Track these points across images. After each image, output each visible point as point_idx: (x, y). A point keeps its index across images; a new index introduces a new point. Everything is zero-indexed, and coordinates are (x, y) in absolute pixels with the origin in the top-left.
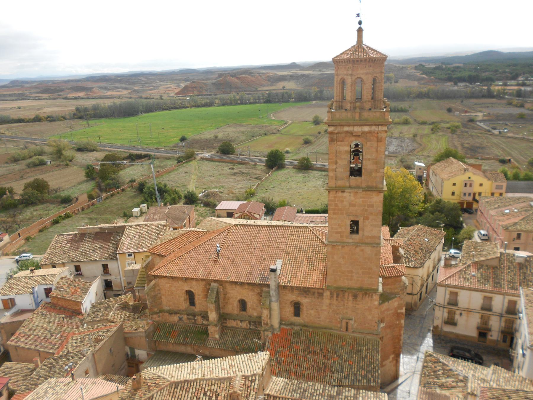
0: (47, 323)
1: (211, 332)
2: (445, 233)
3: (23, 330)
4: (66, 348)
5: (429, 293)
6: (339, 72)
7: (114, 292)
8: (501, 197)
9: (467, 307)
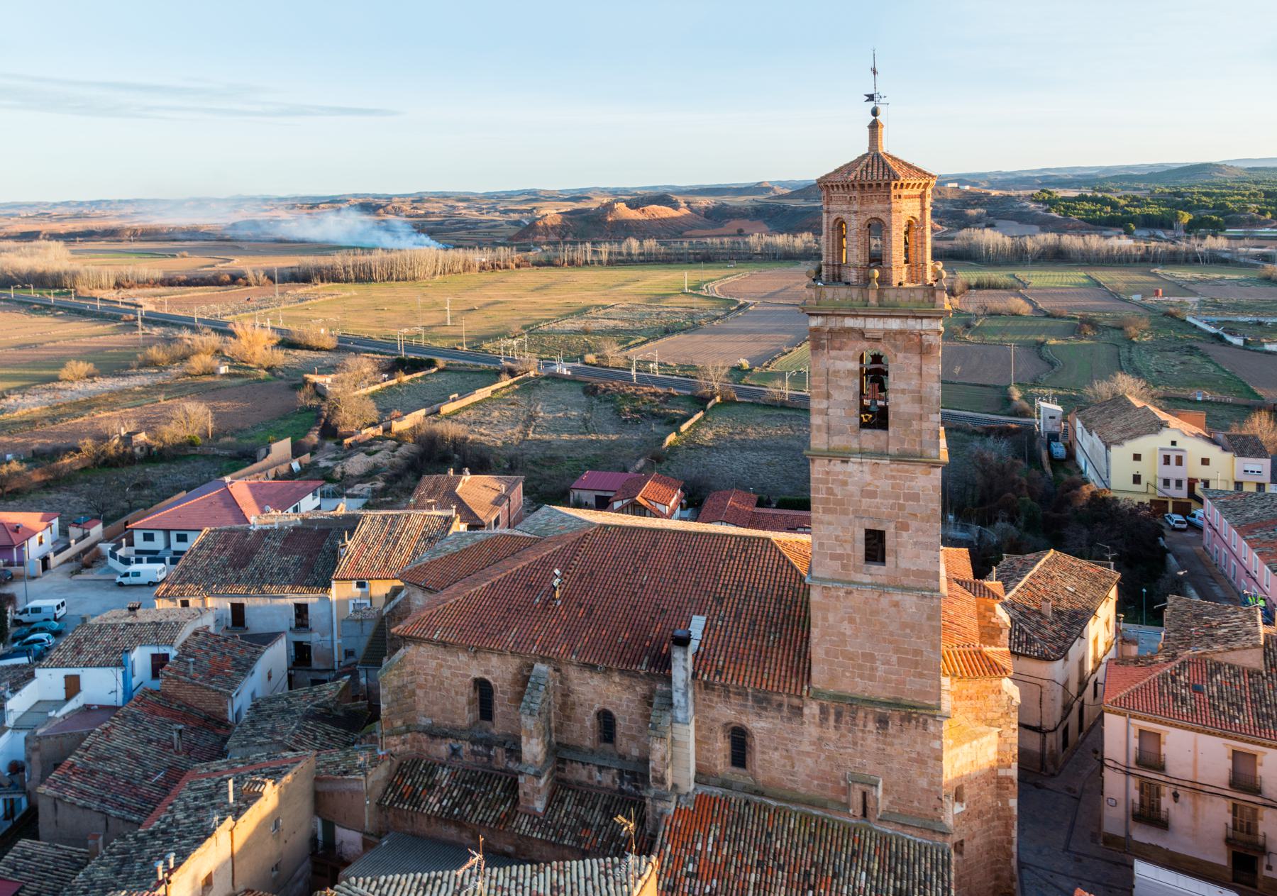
0: (142, 742)
1: (525, 793)
2: (1119, 575)
3: (82, 757)
4: (171, 812)
5: (1089, 730)
6: (831, 207)
7: (313, 673)
8: (1260, 494)
9: (1190, 777)
